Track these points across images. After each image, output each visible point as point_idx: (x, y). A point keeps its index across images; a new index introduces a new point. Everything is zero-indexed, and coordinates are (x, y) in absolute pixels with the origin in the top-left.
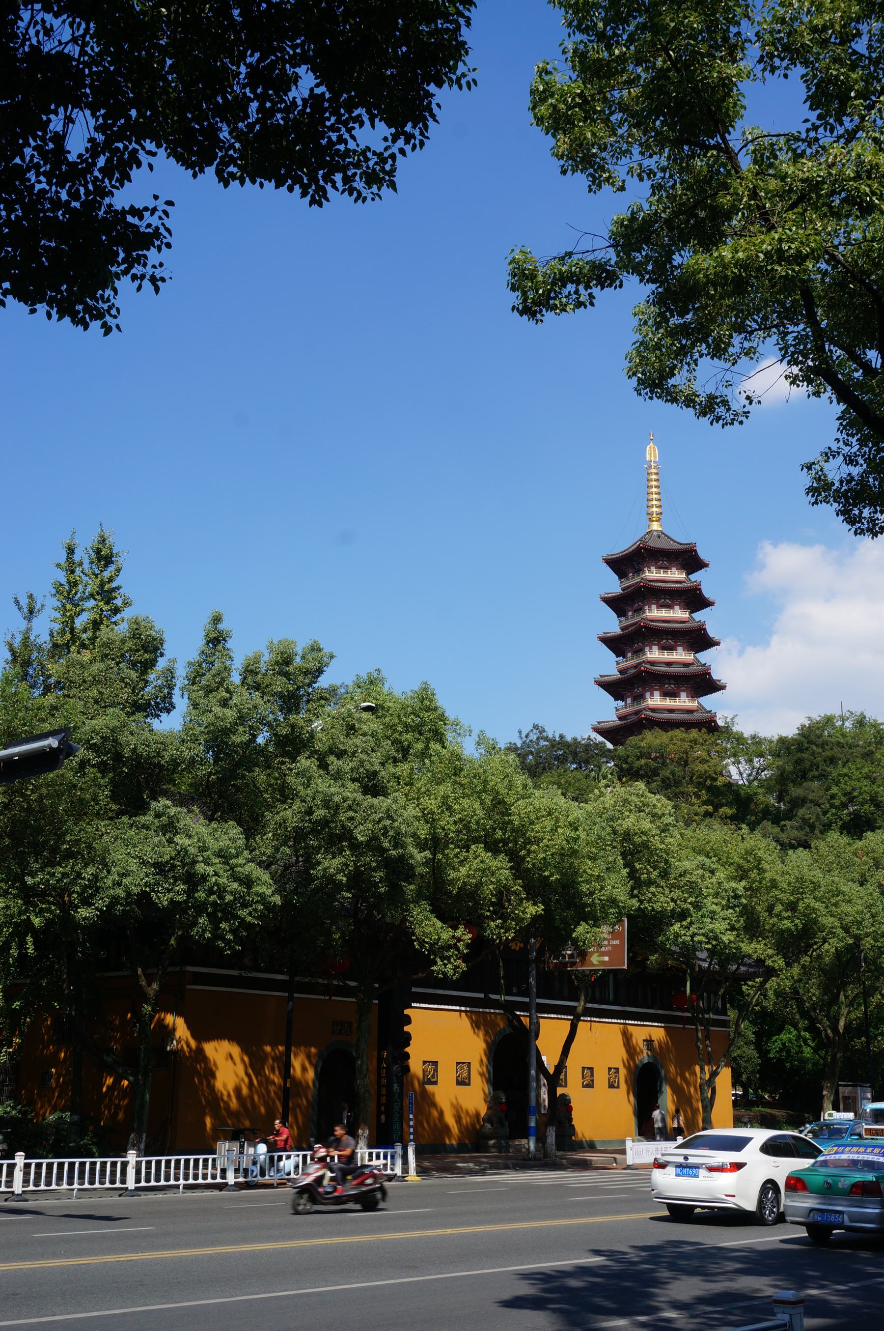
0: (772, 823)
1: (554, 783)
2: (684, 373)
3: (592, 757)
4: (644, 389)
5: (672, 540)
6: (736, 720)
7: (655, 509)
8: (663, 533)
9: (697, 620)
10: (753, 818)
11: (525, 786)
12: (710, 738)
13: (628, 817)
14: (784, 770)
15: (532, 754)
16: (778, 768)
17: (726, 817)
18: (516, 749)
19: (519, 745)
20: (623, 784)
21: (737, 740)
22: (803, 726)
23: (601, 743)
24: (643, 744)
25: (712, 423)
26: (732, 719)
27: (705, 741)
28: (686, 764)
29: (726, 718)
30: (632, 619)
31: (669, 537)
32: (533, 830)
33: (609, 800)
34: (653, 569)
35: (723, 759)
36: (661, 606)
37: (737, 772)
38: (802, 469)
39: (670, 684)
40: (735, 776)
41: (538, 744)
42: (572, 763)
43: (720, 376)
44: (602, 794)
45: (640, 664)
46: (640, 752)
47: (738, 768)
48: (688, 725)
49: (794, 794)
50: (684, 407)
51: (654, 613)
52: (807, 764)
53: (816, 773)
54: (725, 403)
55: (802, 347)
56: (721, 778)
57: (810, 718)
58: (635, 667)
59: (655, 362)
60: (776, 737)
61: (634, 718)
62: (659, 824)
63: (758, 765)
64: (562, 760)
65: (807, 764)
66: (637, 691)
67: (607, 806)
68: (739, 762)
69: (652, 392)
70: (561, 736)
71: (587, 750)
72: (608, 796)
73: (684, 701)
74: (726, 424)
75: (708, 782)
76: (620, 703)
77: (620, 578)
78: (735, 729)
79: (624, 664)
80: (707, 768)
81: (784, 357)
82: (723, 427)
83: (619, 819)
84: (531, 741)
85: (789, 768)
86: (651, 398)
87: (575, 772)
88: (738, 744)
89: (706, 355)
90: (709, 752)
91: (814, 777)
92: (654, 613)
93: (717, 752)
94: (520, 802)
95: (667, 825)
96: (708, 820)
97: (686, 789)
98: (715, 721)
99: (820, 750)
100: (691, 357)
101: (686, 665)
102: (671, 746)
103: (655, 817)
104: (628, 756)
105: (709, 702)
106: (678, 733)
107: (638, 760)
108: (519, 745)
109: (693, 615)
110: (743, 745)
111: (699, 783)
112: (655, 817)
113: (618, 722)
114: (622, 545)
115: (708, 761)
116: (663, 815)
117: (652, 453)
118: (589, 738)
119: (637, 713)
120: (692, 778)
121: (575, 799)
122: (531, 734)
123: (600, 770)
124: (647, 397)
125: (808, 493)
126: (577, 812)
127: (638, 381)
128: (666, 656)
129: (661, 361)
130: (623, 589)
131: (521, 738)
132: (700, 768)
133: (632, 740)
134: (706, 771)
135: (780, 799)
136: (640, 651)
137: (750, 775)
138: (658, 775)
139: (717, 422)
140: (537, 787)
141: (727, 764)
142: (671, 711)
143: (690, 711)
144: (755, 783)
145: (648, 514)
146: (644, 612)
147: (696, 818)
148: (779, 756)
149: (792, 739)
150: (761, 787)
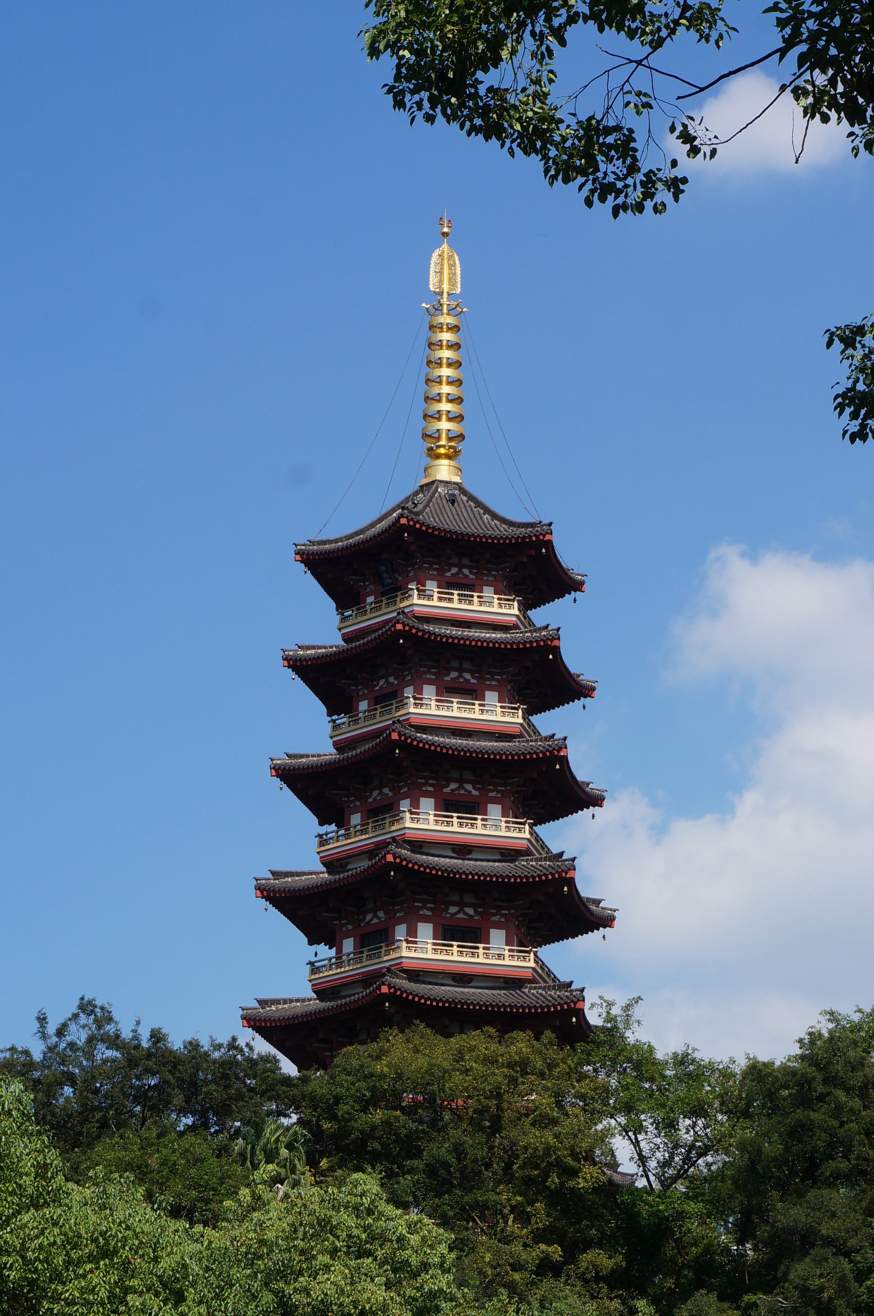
0: (721, 1299)
1: (129, 1167)
2: (525, 60)
3: (240, 1097)
4: (413, 92)
5: (487, 511)
6: (637, 1012)
7: (444, 425)
8: (464, 492)
9: (544, 733)
10: (670, 1283)
11: (42, 1170)
12: (565, 1058)
13: (327, 1268)
14: (759, 1151)
15: (73, 1084)
16: (742, 1146)
17: (598, 1278)
18: (30, 1065)
19: (37, 1056)
20: (321, 1178)
21: (637, 1066)
22: (815, 1037)
23: (266, 1059)
24: (380, 1067)
25: (589, 203)
26: (627, 1008)
27: (550, 1067)
28: (497, 1126)
29: (610, 1004)
30: (368, 720)
31: (478, 504)
32: (56, 1298)
33: (275, 1219)
34: (432, 586)
35: (594, 1116)
36: (447, 690)
37: (630, 1154)
38: (829, 344)
39: (462, 905)
40: (628, 1165)
41: (90, 1056)
42: (183, 1111)
43: (618, 77)
44: (258, 1203)
45: (382, 846)
46: (373, 1089)
47: (636, 1144)
48: (505, 1020)
49: (783, 1221)
50: (518, 151)
51: (429, 707)
52: (820, 1141)
53: (843, 1165)
54: (626, 148)
55: (837, 22)
56: (588, 1171)
57: (832, 1016)
58: (371, 852)
59: (447, 21)
60: (742, 1063)
61: (359, 994)
62: (410, 1292)
63: (689, 1138)
64: (155, 1103)
65: (820, 1141)
66: (374, 919)
67: (270, 1235)
68: (639, 1128)
69: (434, 102)
70: (157, 1036)
71: (225, 1076)
72: (276, 1208)
73: (497, 954)
74: (624, 207)
75: (554, 1180)
76: (325, 952)
77: (341, 606)
78: (632, 1037)
79: (341, 845)
80: (552, 1141)
81: (790, 43)
82: (616, 214)
83: (300, 1273)
84: (72, 1045)
85: (772, 1148)
86: (430, 118)
87: (190, 1138)
88: (640, 1077)
89: (586, 19)
90: (559, 1097)
91: (837, 1175)
92: (429, 707)
93: (582, 1097)
94: (26, 1217)
95: (433, 1295)
96: (547, 1284)
97: (492, 1196)
98: (580, 1014)
99: (857, 1103)
100: (548, 20)
101: (509, 854)
102: (457, 1077)
103: (400, 1272)
104: (337, 1099)
105: (567, 958)
106: (479, 1041)
107: (365, 1110)
108: (37, 1056)
109: (534, 719)
110: (652, 1080)
111: (528, 1181)
112: (400, 1272)
113: (316, 1005)
114: (352, 513)
115: (554, 1122)
116: (425, 1266)
117: (444, 272)
118: (233, 1045)
119: (370, 979)
120: (508, 1166)
121: (175, 1212)
122: (73, 1027)
123: (259, 1135)
124: (420, 115)
125: (841, 408)
126: (184, 1246)
127: (399, 66)
128: (456, 828)
129: (464, 20)
130: (347, 638)
131: (44, 1036)
132: (534, 1138)
133: (353, 1055)
134: (548, 1150)
135: (743, 1233)
136: (387, 810)
137: (665, 1164)
138: (417, 1154)
139: (603, 199)
140: (76, 1175)
141: (608, 1133)
142: (462, 978)
143: (513, 983)
144: (681, 1187)
145: (425, 436)
146: (402, 705)
147: (517, 1276)
148: (746, 1114)
149: (784, 1068)
150: (694, 1198)
